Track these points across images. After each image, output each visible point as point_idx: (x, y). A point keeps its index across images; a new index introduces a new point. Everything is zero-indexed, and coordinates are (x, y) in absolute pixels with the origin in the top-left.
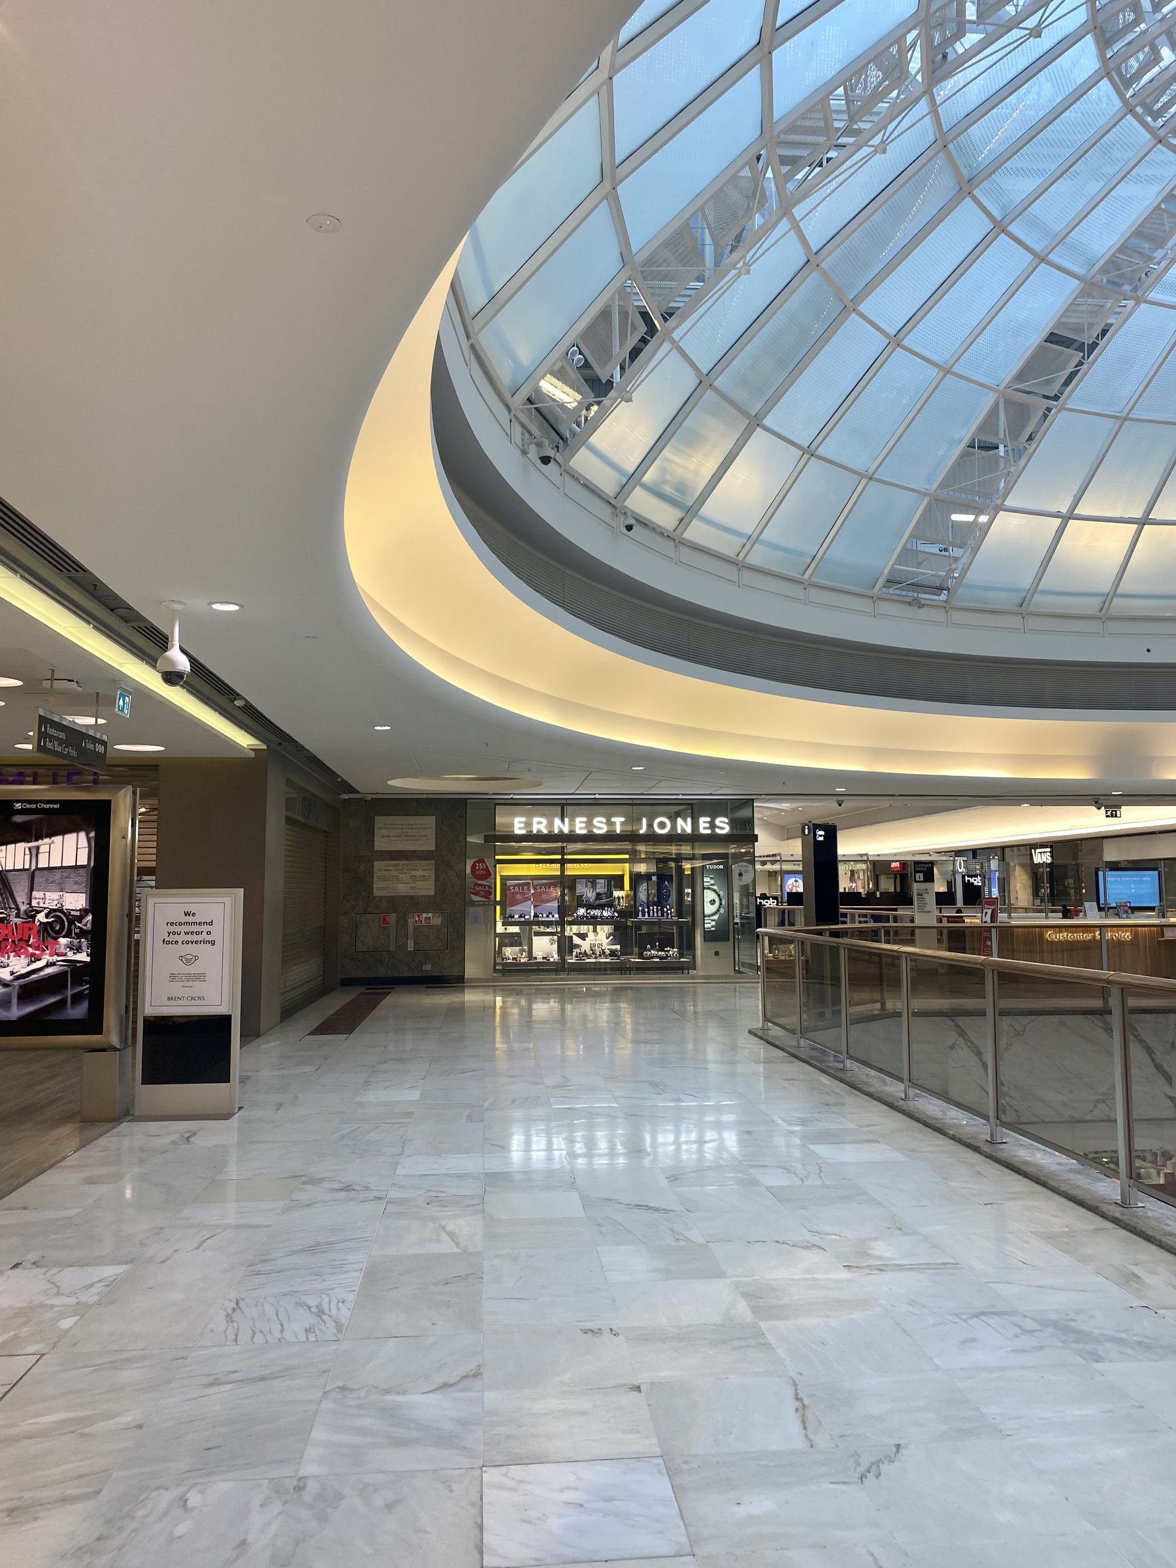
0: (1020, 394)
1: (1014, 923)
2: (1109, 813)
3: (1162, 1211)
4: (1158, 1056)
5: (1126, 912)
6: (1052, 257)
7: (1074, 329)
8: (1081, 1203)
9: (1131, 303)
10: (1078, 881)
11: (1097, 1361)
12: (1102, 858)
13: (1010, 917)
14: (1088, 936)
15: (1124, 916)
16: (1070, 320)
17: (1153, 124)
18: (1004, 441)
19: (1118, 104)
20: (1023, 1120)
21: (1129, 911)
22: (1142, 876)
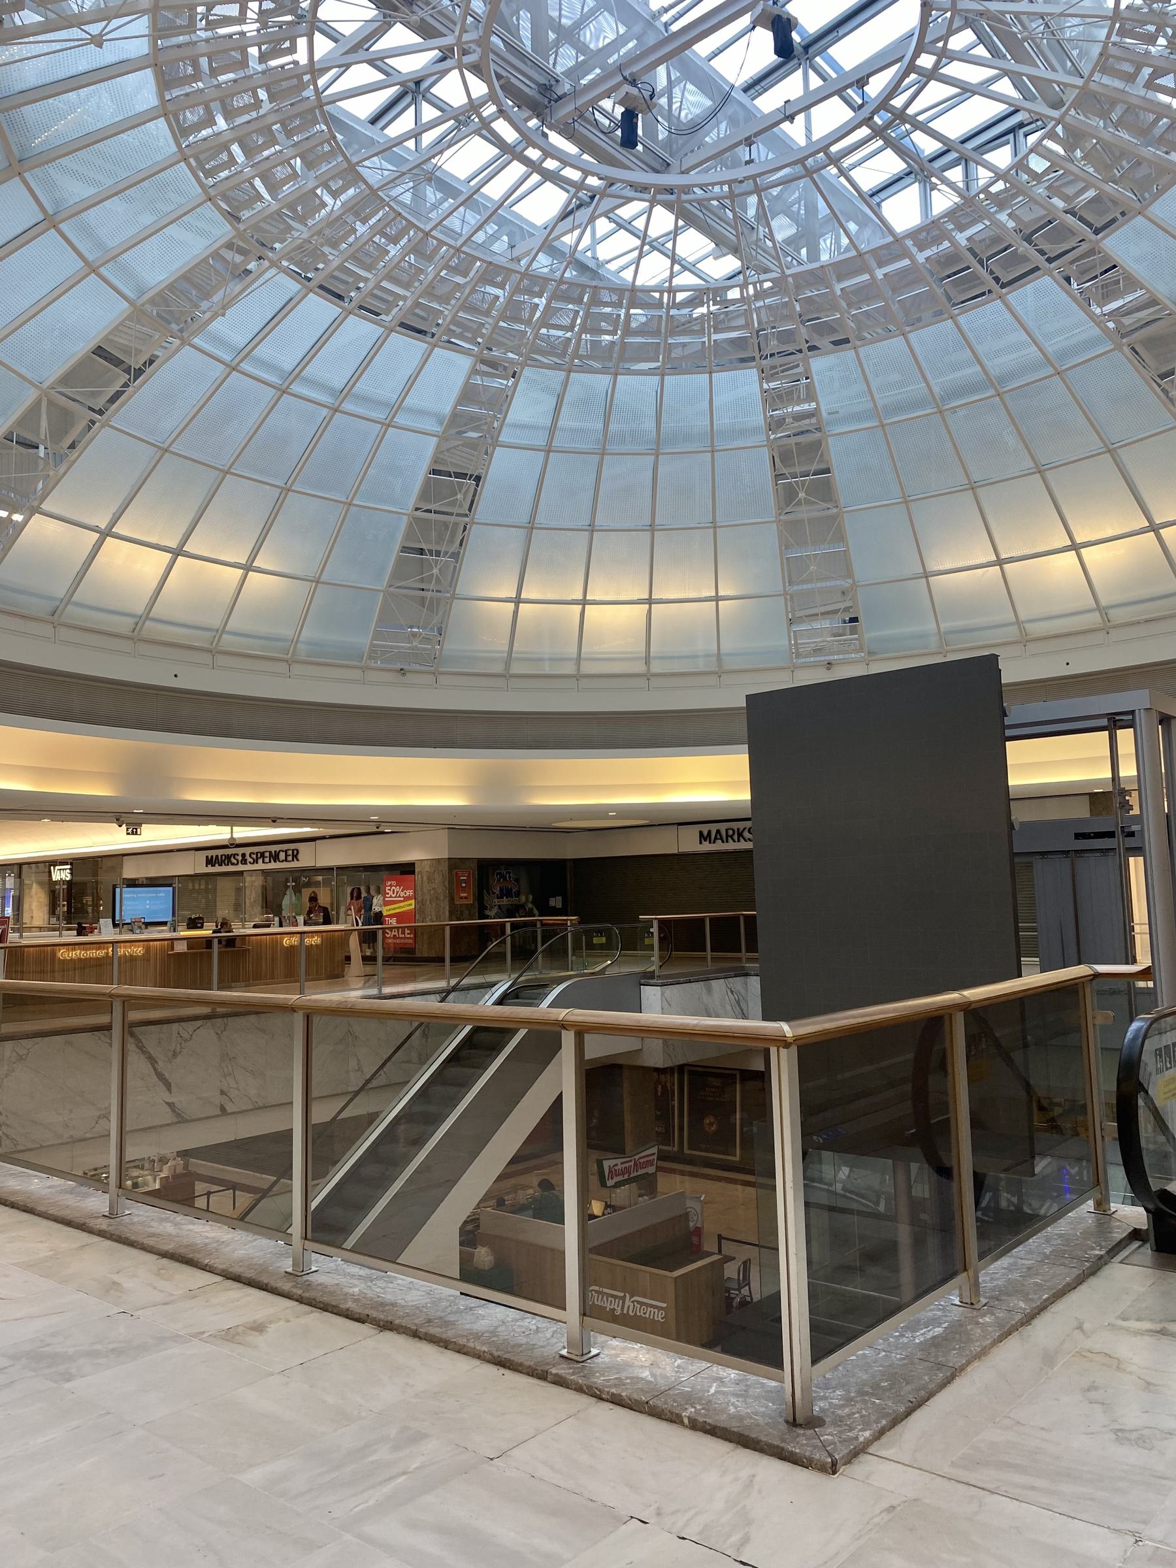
0: (64, 398)
1: (24, 942)
2: (130, 831)
3: (146, 1214)
4: (161, 1066)
5: (140, 927)
6: (103, 270)
7: (121, 349)
8: (68, 1223)
9: (177, 342)
10: (97, 898)
11: (69, 1380)
12: (121, 873)
13: (21, 937)
14: (101, 953)
15: (138, 931)
16: (115, 339)
17: (204, 180)
18: (44, 442)
19: (174, 149)
20: (20, 1148)
21: (143, 926)
22: (138, 893)
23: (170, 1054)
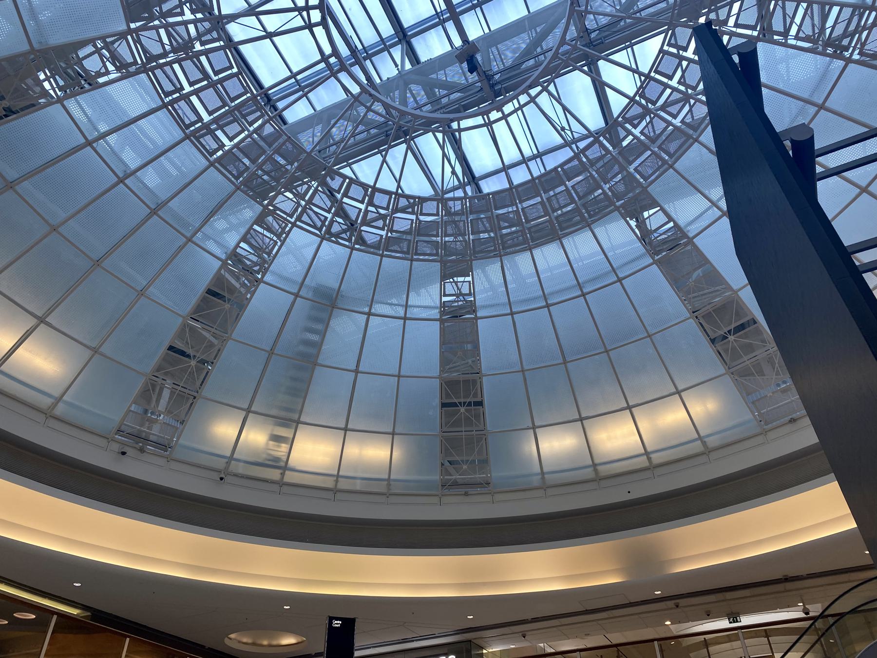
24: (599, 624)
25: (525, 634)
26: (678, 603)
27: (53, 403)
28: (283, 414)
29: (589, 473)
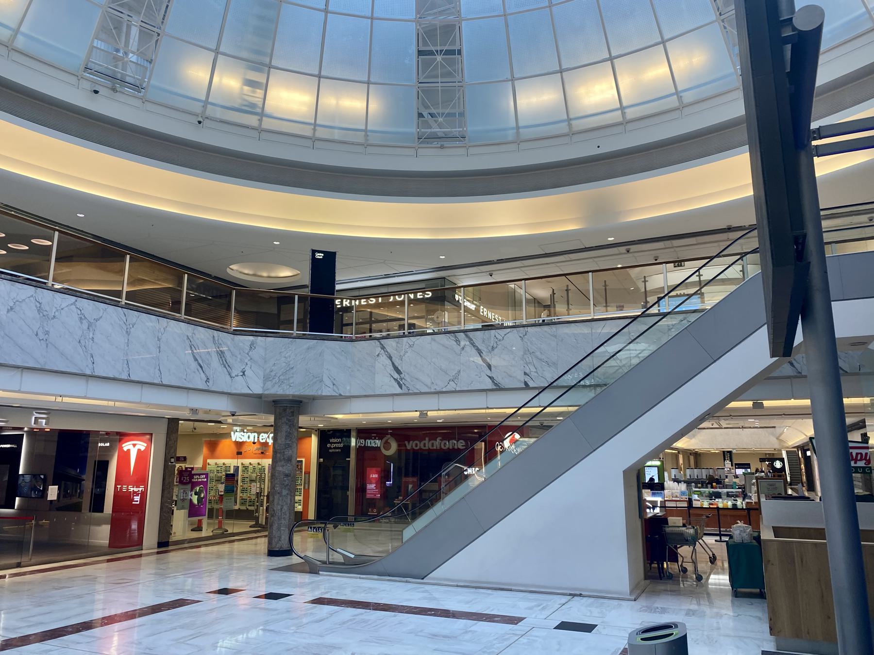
23: (490, 348)
24: (558, 266)
25: (492, 273)
26: (629, 249)
27: (11, 35)
28: (252, 57)
29: (563, 128)
